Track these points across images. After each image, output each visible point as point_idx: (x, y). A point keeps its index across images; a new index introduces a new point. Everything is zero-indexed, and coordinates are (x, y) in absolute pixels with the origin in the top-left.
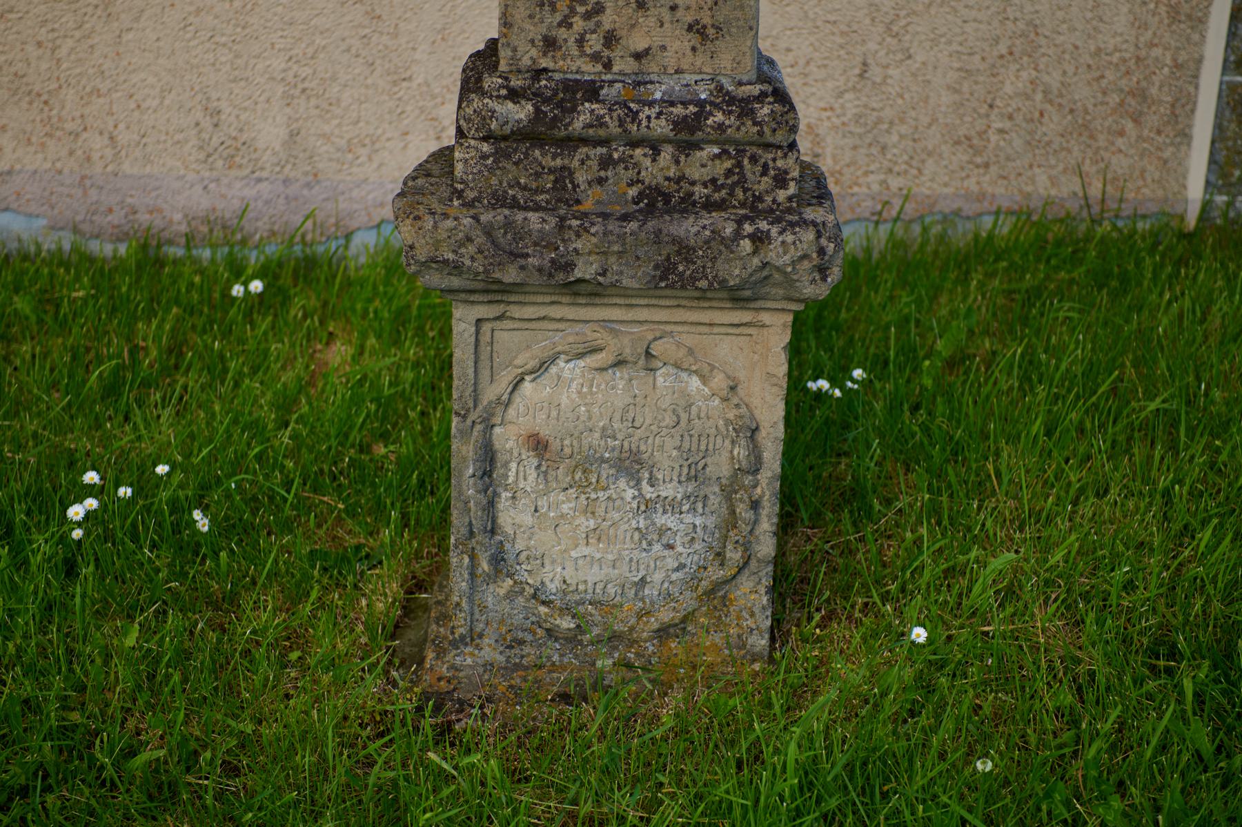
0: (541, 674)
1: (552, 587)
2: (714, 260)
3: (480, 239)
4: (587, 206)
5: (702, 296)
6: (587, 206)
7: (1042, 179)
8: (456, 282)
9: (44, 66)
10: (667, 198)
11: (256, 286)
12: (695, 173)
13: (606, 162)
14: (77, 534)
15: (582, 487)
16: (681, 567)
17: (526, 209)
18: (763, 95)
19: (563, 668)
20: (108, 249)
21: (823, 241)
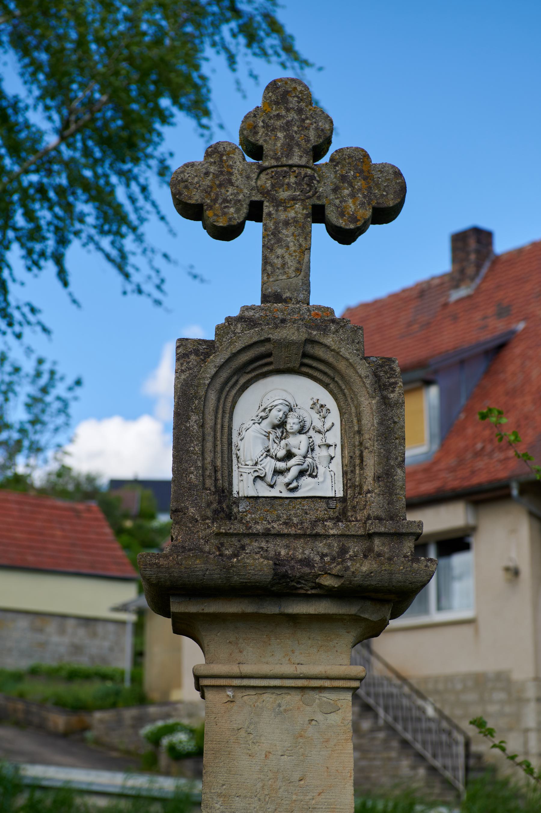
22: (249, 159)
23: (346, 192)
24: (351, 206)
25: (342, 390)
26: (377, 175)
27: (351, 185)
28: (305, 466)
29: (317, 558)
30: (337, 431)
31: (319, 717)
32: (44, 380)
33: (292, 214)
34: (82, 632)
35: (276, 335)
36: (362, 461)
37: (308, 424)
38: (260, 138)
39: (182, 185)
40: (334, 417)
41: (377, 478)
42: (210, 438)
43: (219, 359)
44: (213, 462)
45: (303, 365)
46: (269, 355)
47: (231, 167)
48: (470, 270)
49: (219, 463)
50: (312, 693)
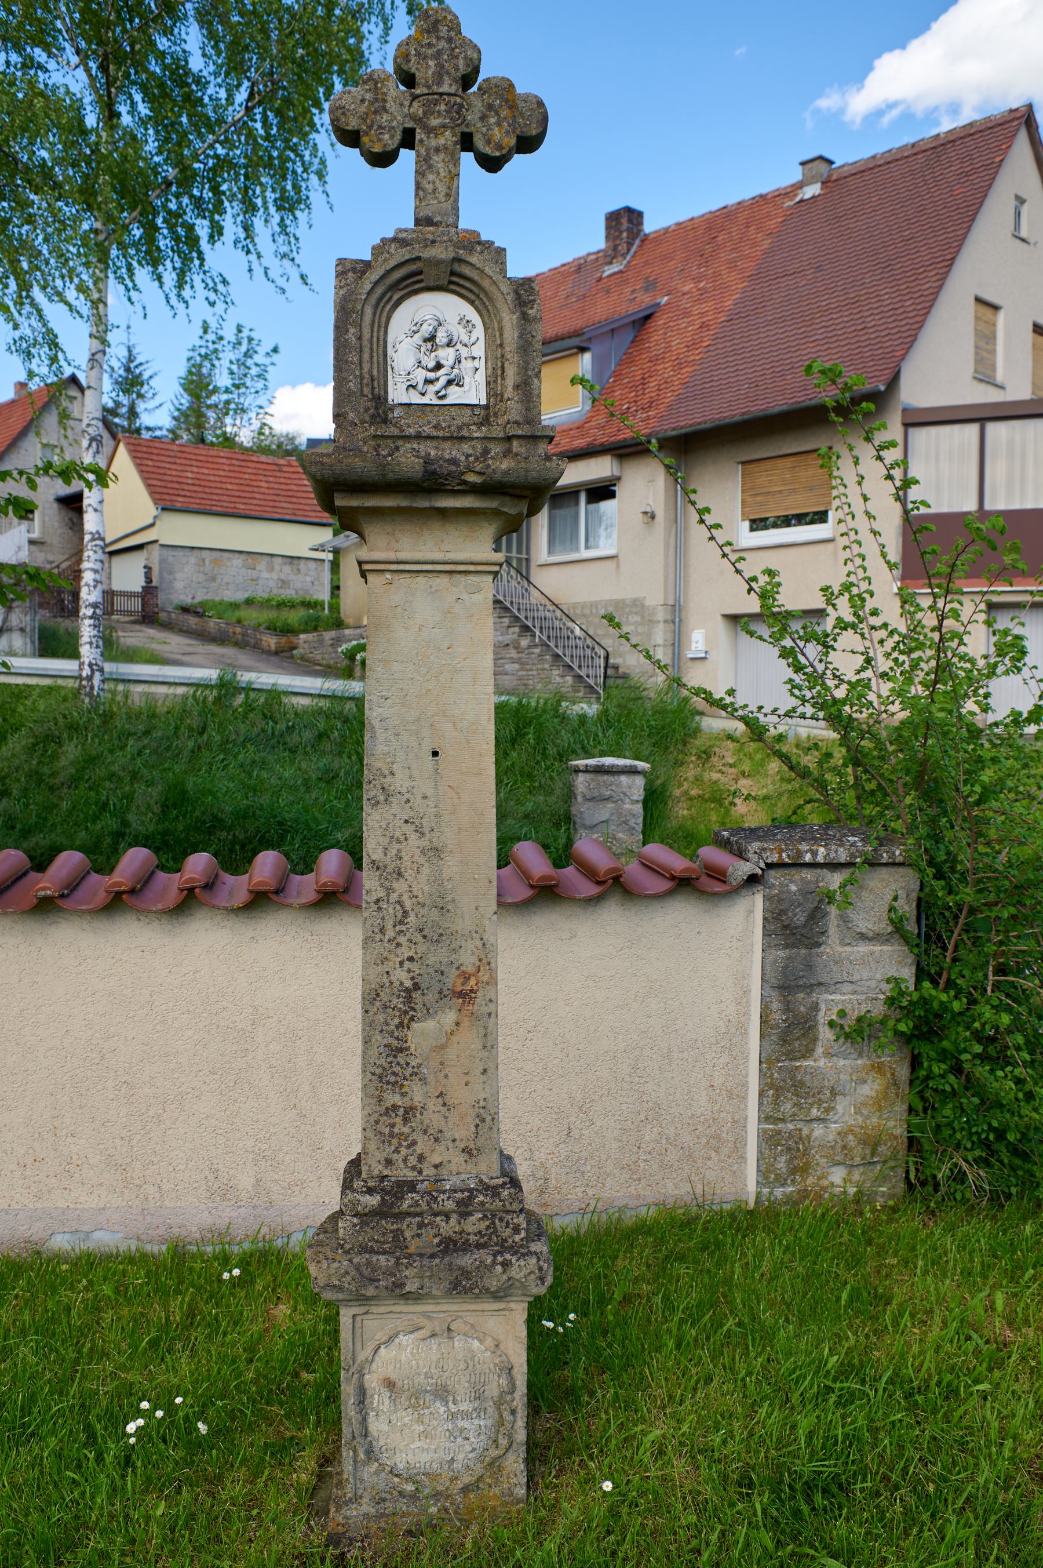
0: (396, 1519)
1: (401, 1466)
2: (482, 1277)
3: (353, 1273)
4: (412, 1249)
5: (477, 1297)
6: (412, 1249)
7: (670, 1185)
8: (340, 1296)
9: (124, 1150)
10: (455, 1243)
11: (236, 1272)
12: (470, 1229)
13: (421, 1225)
14: (132, 1440)
15: (415, 1408)
16: (474, 1450)
17: (378, 1253)
18: (505, 1183)
19: (409, 1514)
20: (156, 1249)
21: (541, 1263)
22: (402, 88)
23: (493, 120)
24: (497, 134)
25: (486, 307)
26: (521, 104)
27: (497, 113)
28: (452, 376)
29: (463, 458)
30: (481, 343)
31: (465, 596)
32: (244, 348)
33: (442, 141)
34: (287, 569)
35: (426, 254)
36: (503, 372)
37: (455, 339)
38: (413, 67)
39: (340, 111)
40: (479, 332)
41: (517, 387)
42: (367, 350)
43: (374, 276)
44: (370, 372)
45: (451, 282)
46: (420, 273)
47: (385, 94)
48: (622, 248)
49: (375, 373)
50: (458, 576)
